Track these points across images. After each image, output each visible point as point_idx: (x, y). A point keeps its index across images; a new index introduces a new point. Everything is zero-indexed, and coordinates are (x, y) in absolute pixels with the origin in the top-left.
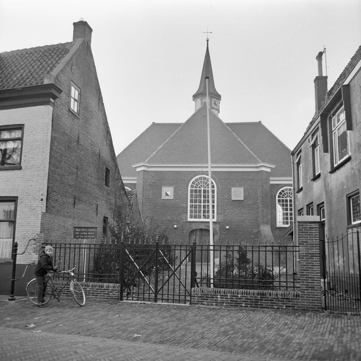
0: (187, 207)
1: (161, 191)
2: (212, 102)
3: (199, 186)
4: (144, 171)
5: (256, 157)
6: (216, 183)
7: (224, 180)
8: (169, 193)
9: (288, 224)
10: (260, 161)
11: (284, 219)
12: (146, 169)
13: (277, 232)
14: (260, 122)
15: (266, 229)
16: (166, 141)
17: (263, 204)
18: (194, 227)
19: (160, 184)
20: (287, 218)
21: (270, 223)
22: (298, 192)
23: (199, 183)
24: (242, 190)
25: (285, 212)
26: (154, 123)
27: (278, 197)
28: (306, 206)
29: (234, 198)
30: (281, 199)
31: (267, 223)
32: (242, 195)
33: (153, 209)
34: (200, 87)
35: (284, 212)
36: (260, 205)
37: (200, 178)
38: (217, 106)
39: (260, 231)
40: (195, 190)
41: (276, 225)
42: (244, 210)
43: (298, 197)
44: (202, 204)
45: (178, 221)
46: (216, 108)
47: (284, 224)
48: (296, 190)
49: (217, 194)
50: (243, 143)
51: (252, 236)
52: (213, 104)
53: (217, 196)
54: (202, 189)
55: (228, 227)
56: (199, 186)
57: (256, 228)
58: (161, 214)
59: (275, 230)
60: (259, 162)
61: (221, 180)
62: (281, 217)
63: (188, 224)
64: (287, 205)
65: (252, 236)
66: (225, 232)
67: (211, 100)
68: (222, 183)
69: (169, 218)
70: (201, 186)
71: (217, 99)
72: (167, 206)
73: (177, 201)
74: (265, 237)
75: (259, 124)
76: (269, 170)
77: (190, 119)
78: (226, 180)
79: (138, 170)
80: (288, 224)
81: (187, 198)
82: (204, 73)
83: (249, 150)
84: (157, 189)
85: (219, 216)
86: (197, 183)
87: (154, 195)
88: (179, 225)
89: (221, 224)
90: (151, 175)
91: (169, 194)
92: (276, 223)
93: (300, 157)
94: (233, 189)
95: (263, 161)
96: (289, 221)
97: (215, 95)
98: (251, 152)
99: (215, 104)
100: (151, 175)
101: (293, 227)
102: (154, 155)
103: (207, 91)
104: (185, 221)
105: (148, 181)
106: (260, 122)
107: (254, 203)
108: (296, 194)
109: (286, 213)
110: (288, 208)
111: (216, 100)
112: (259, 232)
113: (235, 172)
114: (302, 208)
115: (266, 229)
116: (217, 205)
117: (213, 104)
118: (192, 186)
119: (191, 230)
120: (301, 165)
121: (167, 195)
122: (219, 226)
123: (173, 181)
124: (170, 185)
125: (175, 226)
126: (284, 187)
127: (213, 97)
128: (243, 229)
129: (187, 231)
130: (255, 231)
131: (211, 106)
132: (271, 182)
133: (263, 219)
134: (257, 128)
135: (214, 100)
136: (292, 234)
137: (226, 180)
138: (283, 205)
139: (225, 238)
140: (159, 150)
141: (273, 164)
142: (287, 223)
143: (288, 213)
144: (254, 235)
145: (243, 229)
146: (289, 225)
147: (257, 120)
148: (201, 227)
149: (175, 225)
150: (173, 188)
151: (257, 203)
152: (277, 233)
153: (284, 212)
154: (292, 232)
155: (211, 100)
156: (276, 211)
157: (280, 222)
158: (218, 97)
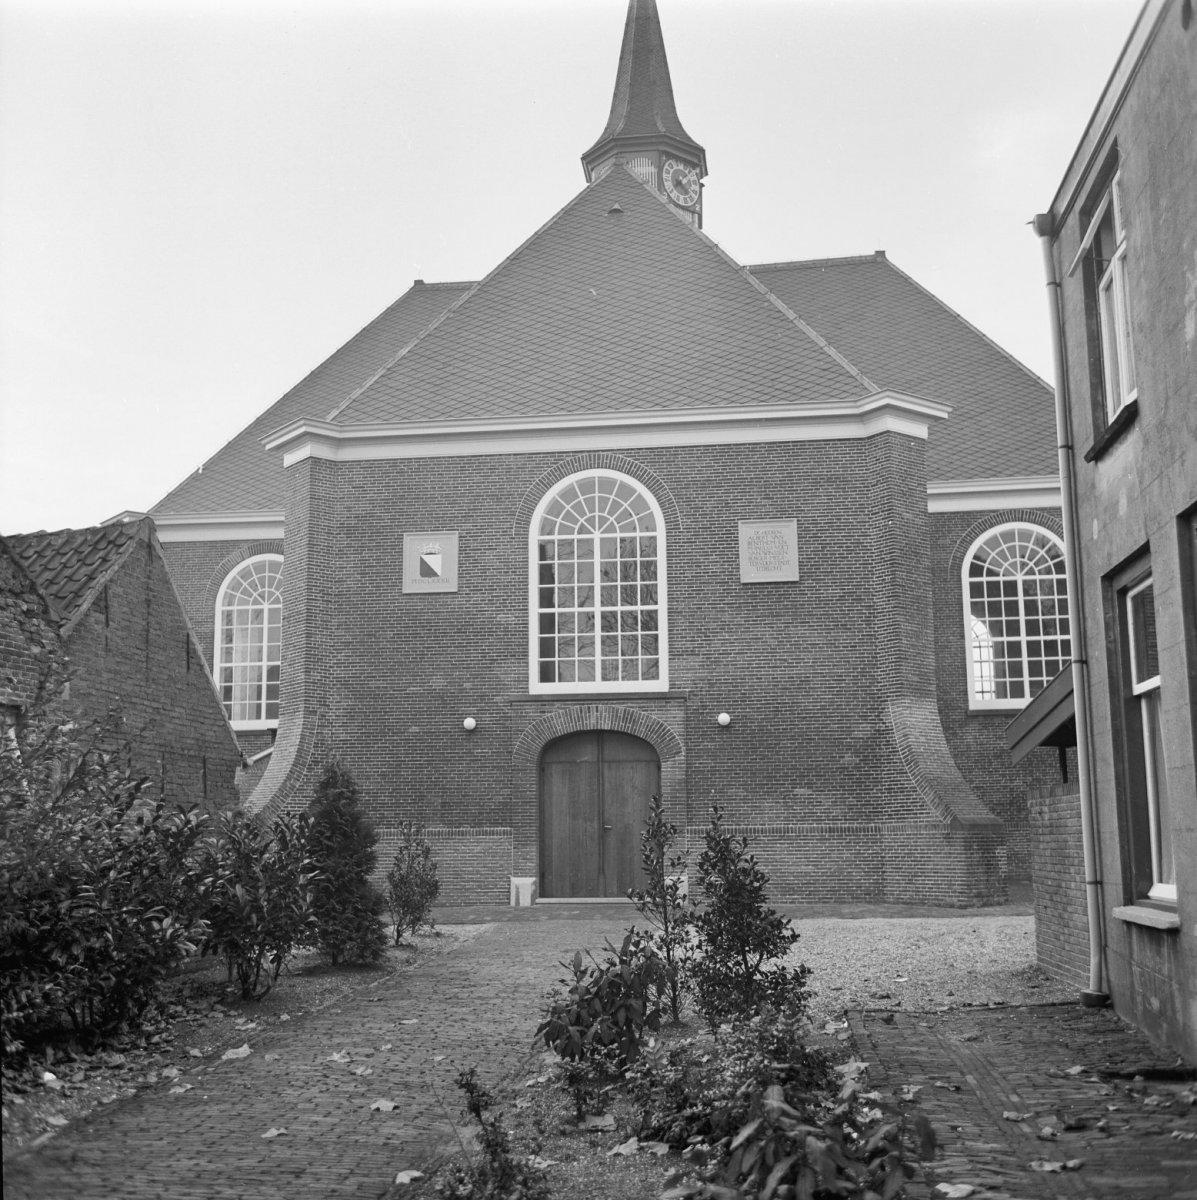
0: (526, 624)
1: (401, 553)
2: (664, 175)
3: (582, 520)
4: (314, 461)
5: (854, 371)
6: (662, 505)
7: (704, 487)
8: (435, 563)
9: (1022, 695)
10: (874, 388)
11: (999, 671)
12: (325, 452)
13: (971, 735)
14: (881, 254)
15: (915, 722)
16: (431, 327)
17: (895, 596)
18: (561, 723)
19: (393, 519)
20: (1016, 670)
21: (933, 688)
22: (1098, 454)
23: (578, 508)
24: (789, 530)
25: (1005, 639)
26: (419, 283)
27: (972, 574)
28: (1173, 530)
29: (749, 574)
30: (984, 579)
31: (920, 692)
32: (793, 555)
33: (362, 642)
34: (610, 119)
35: (1000, 639)
36: (880, 601)
37: (587, 486)
38: (686, 192)
39: (888, 730)
40: (562, 543)
41: (967, 701)
42: (801, 630)
43: (1103, 486)
44: (597, 609)
45: (482, 697)
46: (681, 203)
47: (1001, 692)
48: (1085, 442)
49: (669, 556)
50: (791, 315)
51: (849, 759)
52: (669, 185)
53: (669, 567)
54: (597, 536)
55: (724, 718)
56: (582, 520)
57: (864, 717)
58: (400, 663)
59: (961, 726)
60: (862, 392)
61: (687, 487)
62: (989, 670)
63: (531, 710)
64: (1012, 608)
65: (849, 759)
66: (713, 740)
67: (660, 169)
68: (689, 501)
69: (438, 682)
70: (591, 521)
71: (687, 163)
72: (430, 625)
73: (477, 597)
74: (913, 760)
75: (877, 263)
76: (920, 431)
77: (550, 228)
78: (709, 492)
79: (290, 459)
80: (1022, 695)
81: (525, 582)
82: (630, 58)
83: (822, 342)
84: (378, 547)
85: (676, 663)
86: (568, 507)
87: (363, 574)
88: (487, 717)
89: (694, 704)
90: (351, 481)
91: (437, 569)
92: (965, 692)
93: (1116, 141)
94: (746, 531)
95: (886, 385)
96: (1026, 679)
97: (677, 148)
98: (832, 351)
99: (678, 184)
100: (351, 481)
101: (1072, 691)
102: (371, 388)
103: (645, 122)
104: (514, 694)
105: (339, 507)
106: (881, 254)
107: (850, 594)
108: (1081, 462)
109: (1010, 644)
110: (1016, 602)
111: (681, 167)
112: (882, 734)
113: (754, 447)
114: (1144, 551)
115: (915, 722)
116: (671, 612)
117: (669, 185)
118: (547, 527)
119: (548, 736)
120: (1114, 268)
121: (427, 571)
122: (680, 715)
123: (454, 502)
124: (437, 524)
125: (470, 723)
126: (998, 523)
127: (670, 156)
128: (803, 725)
129: (528, 741)
130: (862, 730)
131: (1102, 888)
132: (934, 507)
133: (898, 671)
134: (872, 274)
135: (672, 167)
136: (1064, 737)
137: (709, 492)
138: (995, 629)
139: (713, 771)
140: (398, 365)
141: (937, 398)
142: (1017, 691)
143: (1019, 644)
144: (857, 753)
145: (803, 725)
146: (1027, 700)
147: (869, 251)
148: (593, 721)
149: (469, 715)
150: (454, 538)
151: (867, 592)
152: (969, 739)
153: (1000, 639)
154: (1068, 727)
155: (660, 169)
156: (963, 637)
157: (982, 688)
158: (694, 157)
